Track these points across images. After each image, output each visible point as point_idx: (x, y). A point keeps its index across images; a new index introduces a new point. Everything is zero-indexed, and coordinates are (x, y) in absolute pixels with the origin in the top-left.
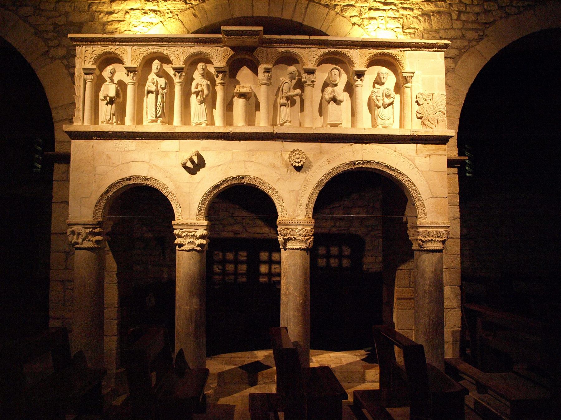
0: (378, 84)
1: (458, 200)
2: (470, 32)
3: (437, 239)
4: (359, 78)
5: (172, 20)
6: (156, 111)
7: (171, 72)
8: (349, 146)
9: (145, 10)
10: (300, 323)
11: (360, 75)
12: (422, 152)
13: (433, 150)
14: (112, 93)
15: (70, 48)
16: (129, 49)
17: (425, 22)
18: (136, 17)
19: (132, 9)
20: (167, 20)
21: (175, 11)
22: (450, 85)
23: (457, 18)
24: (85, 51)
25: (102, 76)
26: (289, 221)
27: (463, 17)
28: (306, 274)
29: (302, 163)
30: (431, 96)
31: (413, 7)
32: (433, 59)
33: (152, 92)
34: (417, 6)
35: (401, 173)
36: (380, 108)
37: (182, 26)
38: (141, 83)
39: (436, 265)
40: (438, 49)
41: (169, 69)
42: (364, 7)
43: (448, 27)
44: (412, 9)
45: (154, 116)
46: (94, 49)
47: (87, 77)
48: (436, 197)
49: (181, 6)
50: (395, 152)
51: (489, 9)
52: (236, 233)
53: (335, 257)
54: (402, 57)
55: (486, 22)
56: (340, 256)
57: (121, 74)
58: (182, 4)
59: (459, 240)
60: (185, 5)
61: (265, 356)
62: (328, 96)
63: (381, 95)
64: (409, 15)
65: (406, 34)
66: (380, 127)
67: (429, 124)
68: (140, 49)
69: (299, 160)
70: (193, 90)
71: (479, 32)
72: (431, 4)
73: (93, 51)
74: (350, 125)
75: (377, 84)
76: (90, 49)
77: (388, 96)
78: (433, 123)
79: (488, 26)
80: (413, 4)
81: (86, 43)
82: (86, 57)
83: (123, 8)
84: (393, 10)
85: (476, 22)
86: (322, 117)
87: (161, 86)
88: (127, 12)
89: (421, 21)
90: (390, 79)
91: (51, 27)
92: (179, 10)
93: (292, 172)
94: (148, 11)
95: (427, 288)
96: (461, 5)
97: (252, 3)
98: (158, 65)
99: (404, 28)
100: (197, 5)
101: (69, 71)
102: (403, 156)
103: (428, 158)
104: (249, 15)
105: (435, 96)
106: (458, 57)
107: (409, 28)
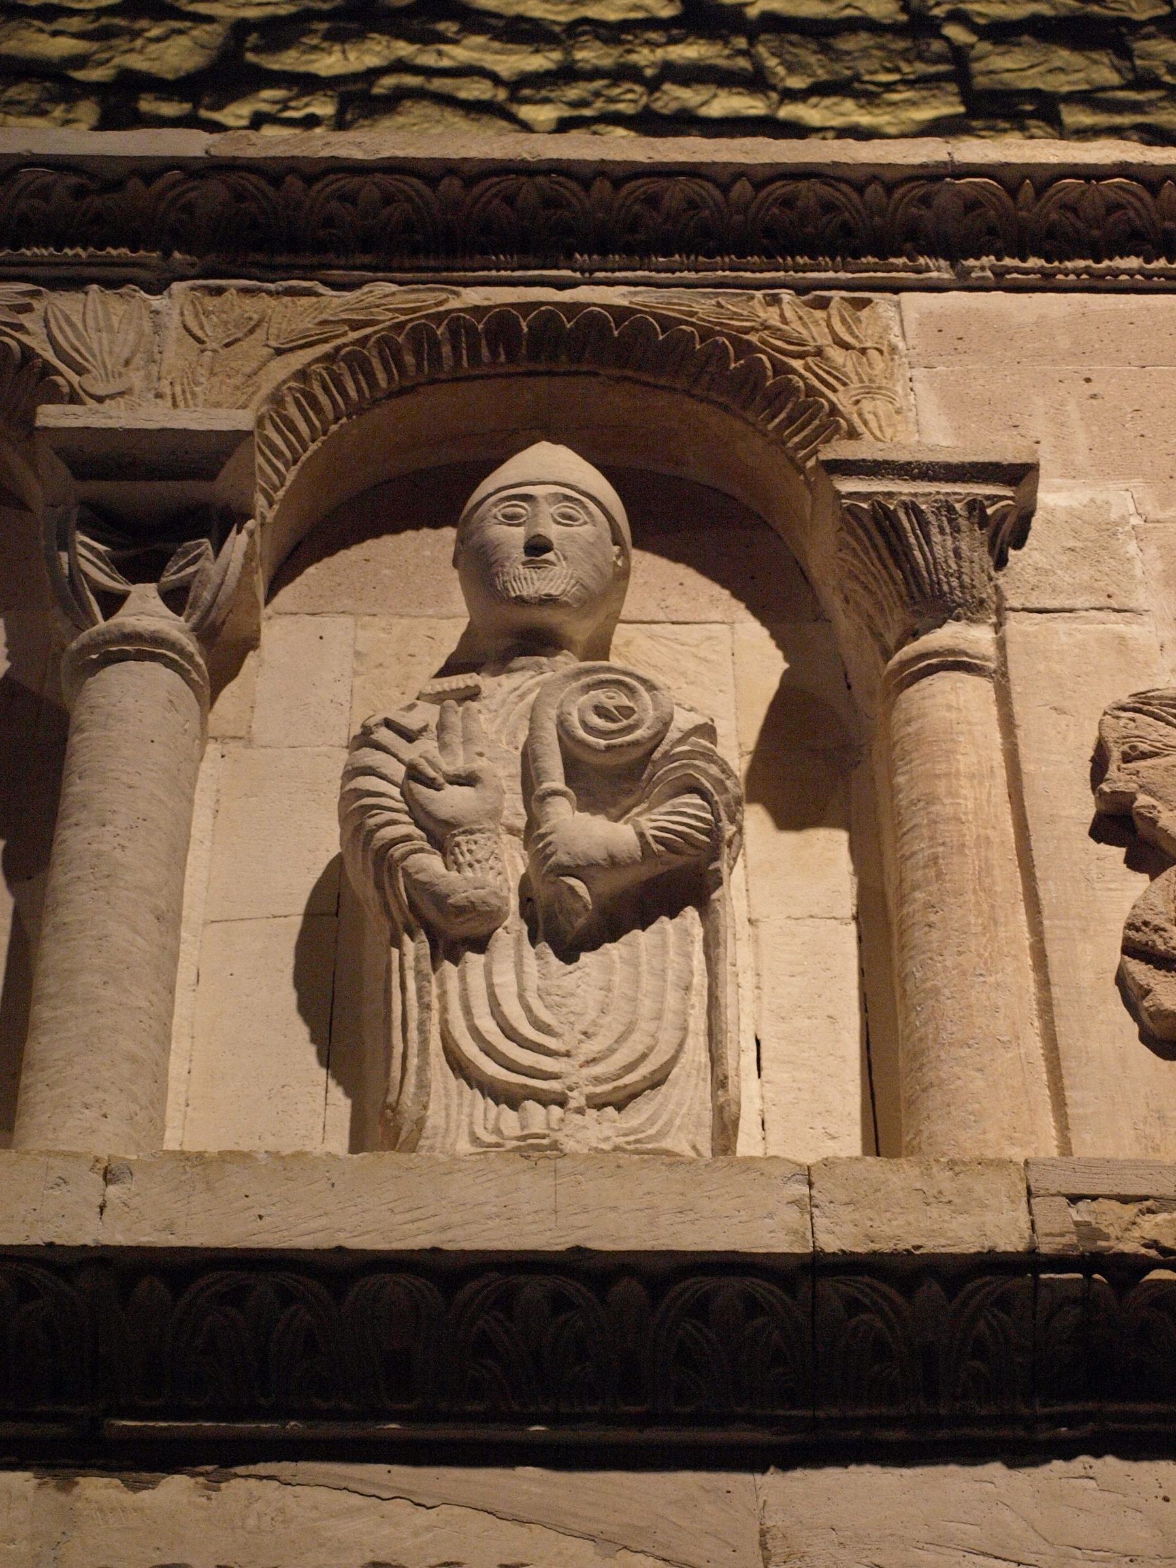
36: (480, 945)
106: (971, 1042)
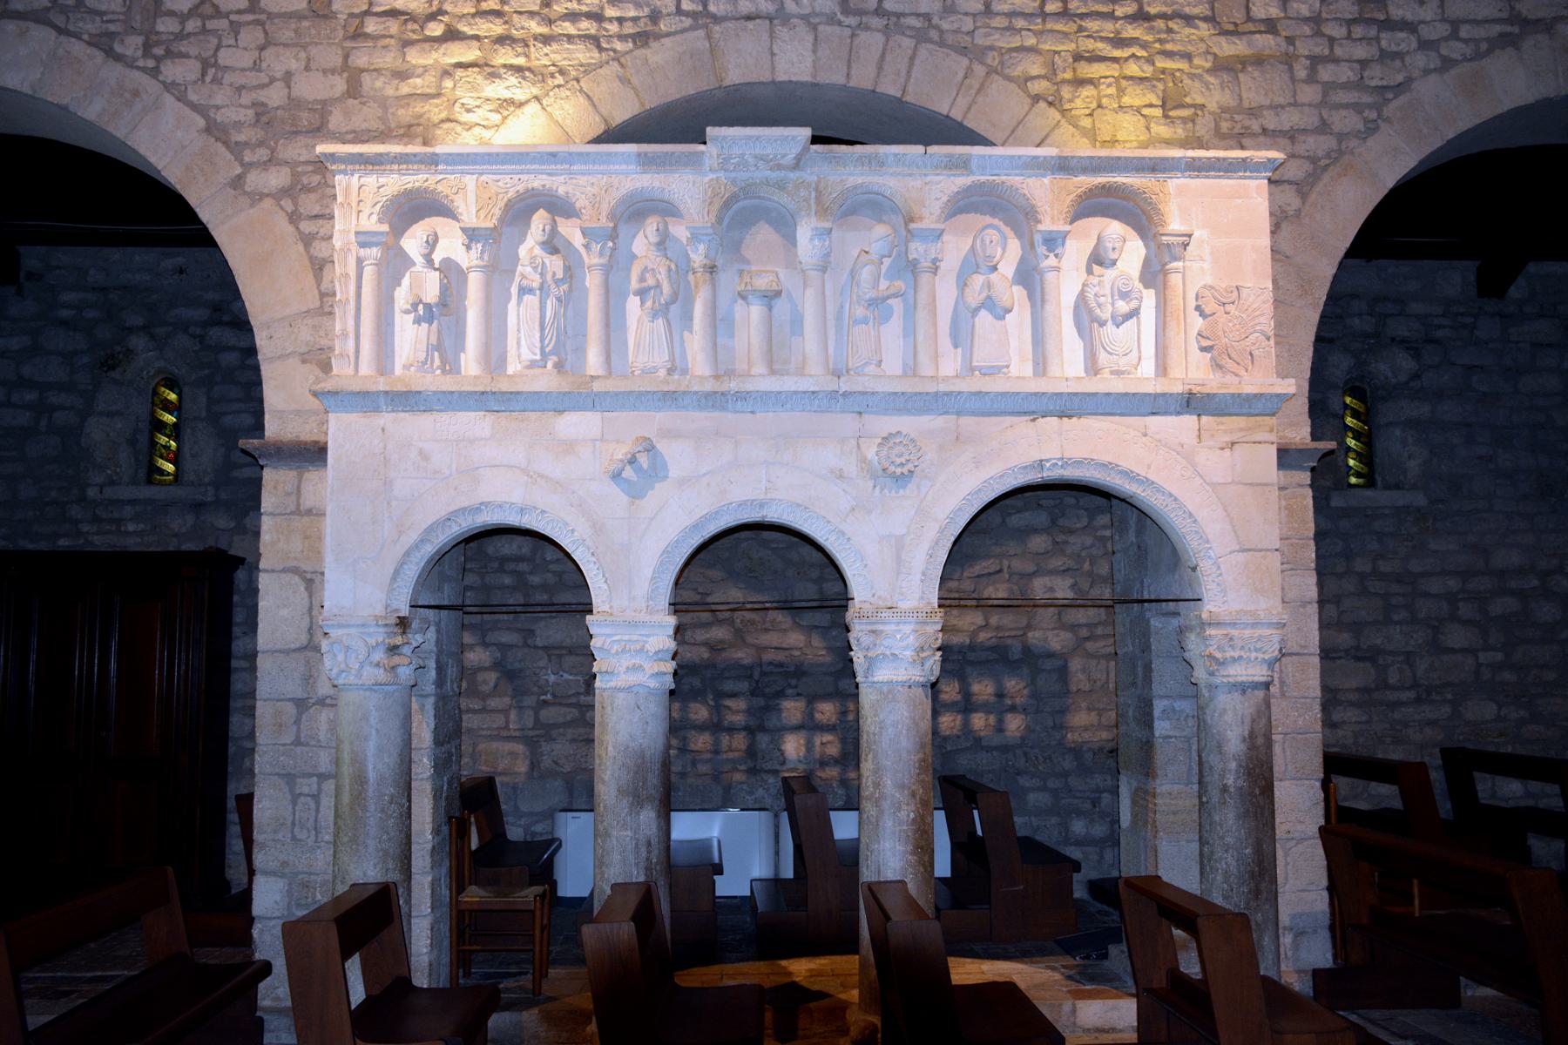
0: (1101, 263)
1: (1314, 555)
2: (1343, 112)
3: (1253, 655)
4: (1050, 250)
5: (564, 93)
6: (542, 339)
7: (578, 240)
8: (1029, 423)
9: (493, 66)
10: (910, 870)
11: (1054, 242)
12: (1213, 436)
13: (1241, 430)
14: (431, 293)
15: (300, 169)
16: (470, 181)
17: (1223, 88)
18: (470, 86)
19: (460, 65)
20: (551, 93)
21: (571, 68)
22: (1288, 254)
23: (1308, 75)
24: (360, 188)
25: (401, 248)
26: (879, 614)
27: (1326, 73)
28: (923, 746)
29: (910, 466)
30: (1236, 293)
31: (1190, 48)
32: (1239, 198)
33: (531, 291)
34: (1202, 48)
35: (1159, 490)
37: (590, 108)
38: (499, 269)
39: (1253, 721)
40: (1251, 172)
41: (571, 232)
42: (1063, 53)
43: (1282, 101)
44: (1188, 57)
45: (538, 352)
46: (382, 180)
47: (362, 252)
48: (1249, 550)
49: (588, 55)
50: (1145, 435)
51: (1394, 48)
52: (714, 647)
53: (986, 708)
54: (1161, 194)
55: (1385, 83)
56: (1000, 705)
57: (452, 246)
58: (589, 50)
59: (1317, 660)
60: (596, 54)
61: (810, 970)
62: (974, 296)
63: (1108, 291)
64: (1179, 70)
65: (1172, 122)
66: (1106, 374)
67: (1230, 364)
68: (498, 181)
69: (903, 460)
70: (634, 284)
71: (1367, 112)
72: (1237, 41)
73: (379, 188)
74: (1028, 370)
75: (1097, 264)
76: (371, 180)
77: (1125, 295)
78: (1238, 360)
79: (1390, 95)
80: (1190, 42)
81: (363, 167)
82: (361, 201)
83: (436, 61)
84: (1138, 58)
85: (1359, 85)
86: (959, 350)
87: (554, 274)
88: (446, 73)
89: (1212, 87)
90: (1133, 253)
91: (251, 112)
92: (581, 66)
93: (886, 491)
94: (503, 71)
95: (1230, 780)
96: (1319, 40)
97: (771, 49)
98: (545, 221)
99: (1168, 107)
100: (627, 53)
101: (297, 229)
102: (1165, 446)
103: (1227, 451)
104: (762, 79)
105: (1244, 292)
107: (1182, 106)
